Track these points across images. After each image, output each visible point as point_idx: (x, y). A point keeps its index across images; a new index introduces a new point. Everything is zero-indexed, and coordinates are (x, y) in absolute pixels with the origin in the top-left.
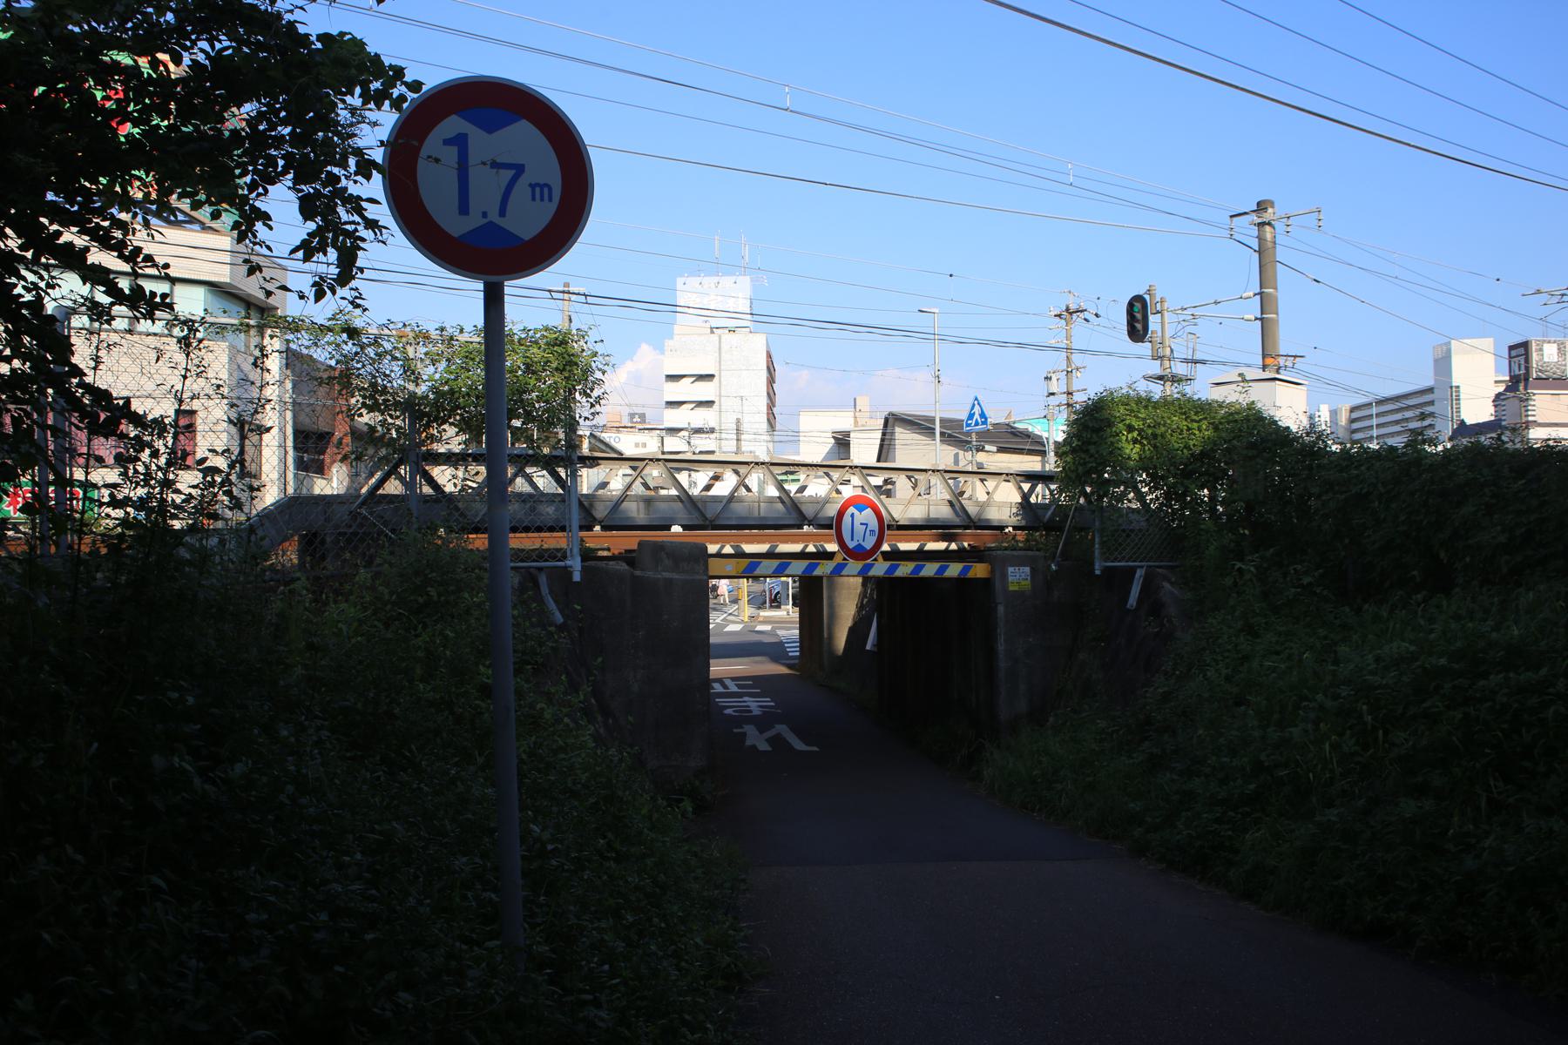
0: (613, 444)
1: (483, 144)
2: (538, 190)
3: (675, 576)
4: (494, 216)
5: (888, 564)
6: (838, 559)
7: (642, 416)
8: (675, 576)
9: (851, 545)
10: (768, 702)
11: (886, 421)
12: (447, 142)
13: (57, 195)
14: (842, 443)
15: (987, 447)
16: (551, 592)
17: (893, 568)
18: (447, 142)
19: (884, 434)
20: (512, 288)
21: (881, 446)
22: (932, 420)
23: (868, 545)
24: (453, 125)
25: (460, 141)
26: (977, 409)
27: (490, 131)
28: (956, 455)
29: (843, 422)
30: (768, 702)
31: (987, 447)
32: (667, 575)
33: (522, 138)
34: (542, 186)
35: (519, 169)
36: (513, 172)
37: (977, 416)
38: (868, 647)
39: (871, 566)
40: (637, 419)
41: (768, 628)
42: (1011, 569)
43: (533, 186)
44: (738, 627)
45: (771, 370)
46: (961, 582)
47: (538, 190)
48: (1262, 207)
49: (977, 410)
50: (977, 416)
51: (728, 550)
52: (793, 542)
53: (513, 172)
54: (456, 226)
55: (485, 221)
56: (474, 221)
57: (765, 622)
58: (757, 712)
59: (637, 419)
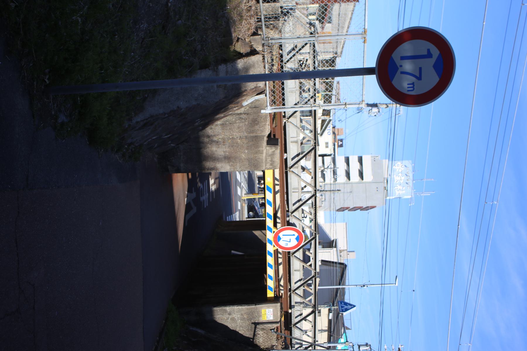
0: (326, 131)
1: (428, 64)
2: (412, 86)
3: (264, 155)
4: (400, 70)
6: (274, 229)
7: (341, 146)
8: (264, 155)
9: (281, 235)
10: (206, 204)
11: (342, 264)
12: (429, 50)
14: (330, 244)
15: (331, 314)
16: (256, 100)
17: (270, 254)
18: (429, 50)
19: (336, 263)
20: (372, 79)
21: (330, 262)
22: (344, 285)
23: (281, 243)
24: (436, 52)
25: (429, 55)
26: (350, 307)
28: (292, 142)
29: (341, 244)
30: (206, 204)
31: (331, 314)
32: (265, 151)
33: (432, 79)
34: (413, 87)
35: (419, 78)
36: (418, 76)
37: (346, 307)
38: (233, 252)
40: (340, 143)
41: (239, 208)
42: (271, 310)
43: (413, 84)
44: (239, 193)
45: (367, 208)
46: (265, 288)
47: (412, 86)
49: (349, 307)
50: (346, 307)
51: (280, 260)
53: (418, 76)
54: (396, 55)
58: (202, 199)
59: (340, 143)
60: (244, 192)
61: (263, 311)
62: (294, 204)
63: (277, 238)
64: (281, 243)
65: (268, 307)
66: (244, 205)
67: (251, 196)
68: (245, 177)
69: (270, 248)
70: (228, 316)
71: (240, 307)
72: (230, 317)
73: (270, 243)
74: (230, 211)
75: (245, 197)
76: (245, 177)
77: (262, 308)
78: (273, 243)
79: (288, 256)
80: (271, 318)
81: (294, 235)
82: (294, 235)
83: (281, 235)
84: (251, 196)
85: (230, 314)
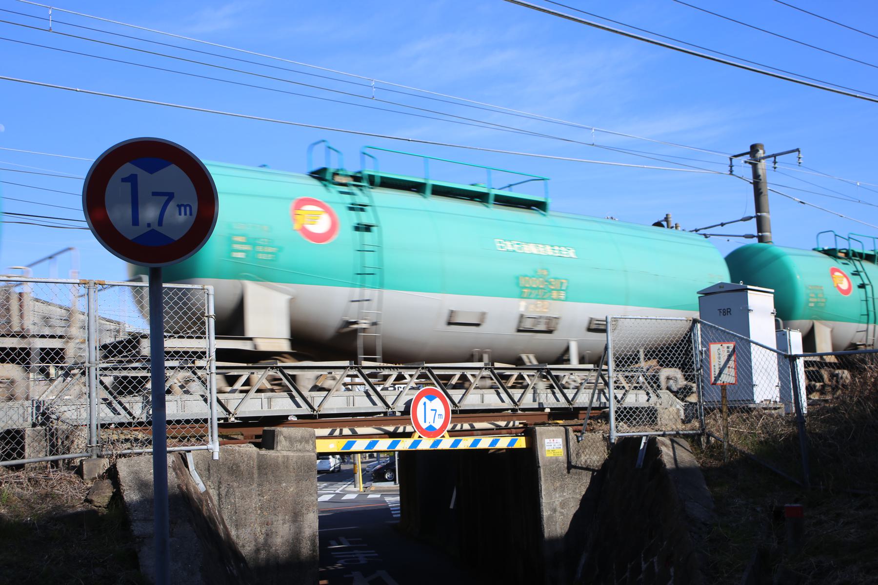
2: (183, 209)
3: (291, 454)
5: (453, 439)
8: (291, 454)
9: (424, 426)
13: (336, 569)
17: (457, 443)
23: (438, 425)
24: (128, 169)
25: (132, 180)
27: (151, 172)
32: (285, 453)
33: (172, 176)
34: (185, 206)
36: (166, 198)
38: (451, 507)
39: (440, 441)
41: (379, 496)
42: (547, 441)
47: (183, 209)
48: (754, 149)
51: (466, 426)
52: (368, 426)
53: (166, 198)
54: (131, 234)
55: (149, 229)
56: (141, 230)
57: (375, 492)
60: (351, 488)
61: (549, 455)
62: (374, 404)
63: (430, 432)
64: (438, 425)
65: (543, 446)
66: (373, 489)
67: (359, 476)
68: (326, 487)
69: (446, 443)
70: (558, 514)
71: (543, 493)
72: (559, 509)
73: (437, 443)
74: (381, 513)
75: (360, 486)
76: (326, 487)
77: (543, 457)
78: (438, 438)
79: (459, 413)
80: (560, 442)
81: (425, 404)
82: (425, 404)
83: (424, 426)
84: (359, 476)
85: (555, 510)
